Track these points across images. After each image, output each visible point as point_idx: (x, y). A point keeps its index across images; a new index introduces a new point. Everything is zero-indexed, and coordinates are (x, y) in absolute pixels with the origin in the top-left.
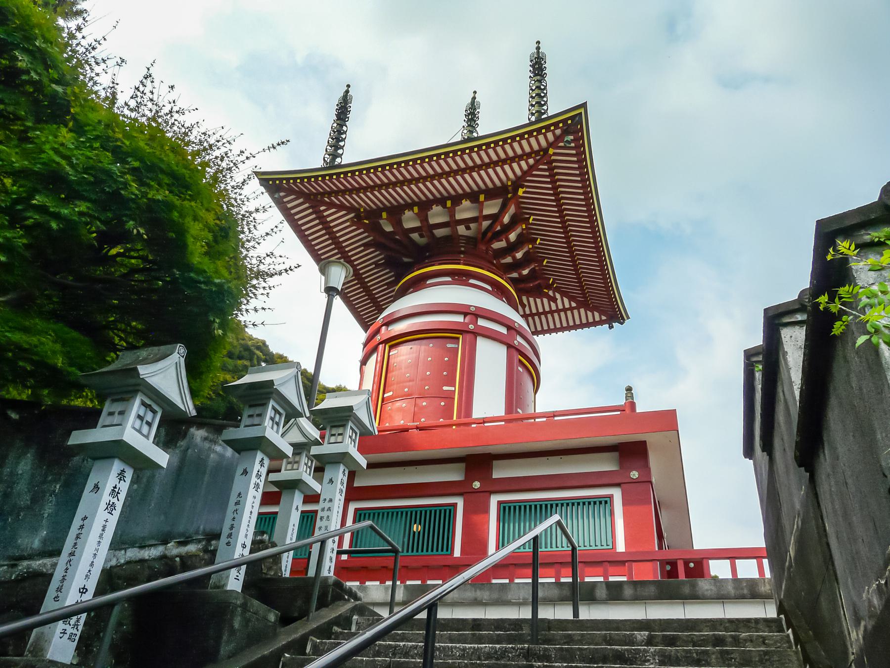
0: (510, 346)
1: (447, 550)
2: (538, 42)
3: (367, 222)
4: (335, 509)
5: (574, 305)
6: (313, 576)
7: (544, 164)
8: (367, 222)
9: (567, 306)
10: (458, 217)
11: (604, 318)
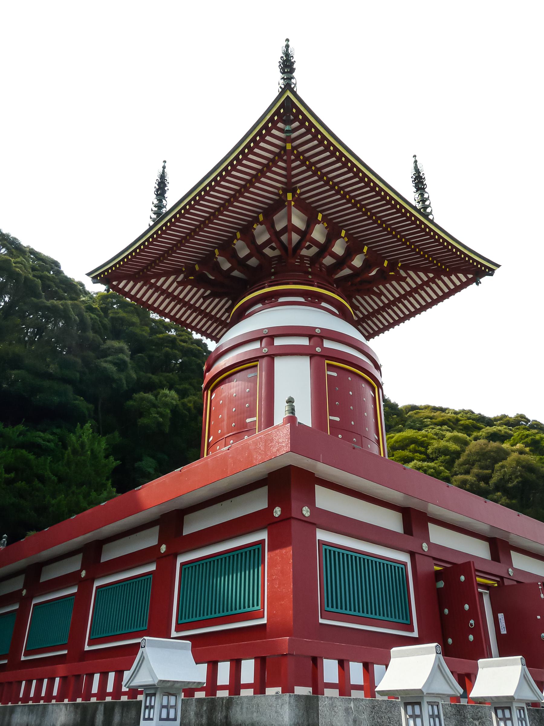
0: (312, 356)
1: (258, 605)
2: (287, 40)
3: (192, 278)
4: (124, 584)
5: (431, 275)
6: (146, 710)
7: (294, 161)
8: (192, 278)
9: (425, 279)
11: (470, 276)
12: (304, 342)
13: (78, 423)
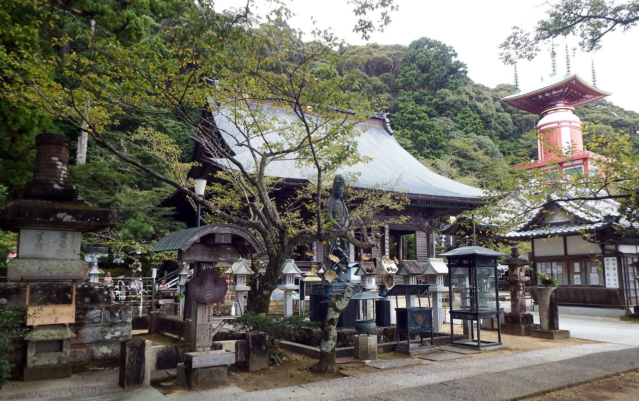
12: (568, 124)
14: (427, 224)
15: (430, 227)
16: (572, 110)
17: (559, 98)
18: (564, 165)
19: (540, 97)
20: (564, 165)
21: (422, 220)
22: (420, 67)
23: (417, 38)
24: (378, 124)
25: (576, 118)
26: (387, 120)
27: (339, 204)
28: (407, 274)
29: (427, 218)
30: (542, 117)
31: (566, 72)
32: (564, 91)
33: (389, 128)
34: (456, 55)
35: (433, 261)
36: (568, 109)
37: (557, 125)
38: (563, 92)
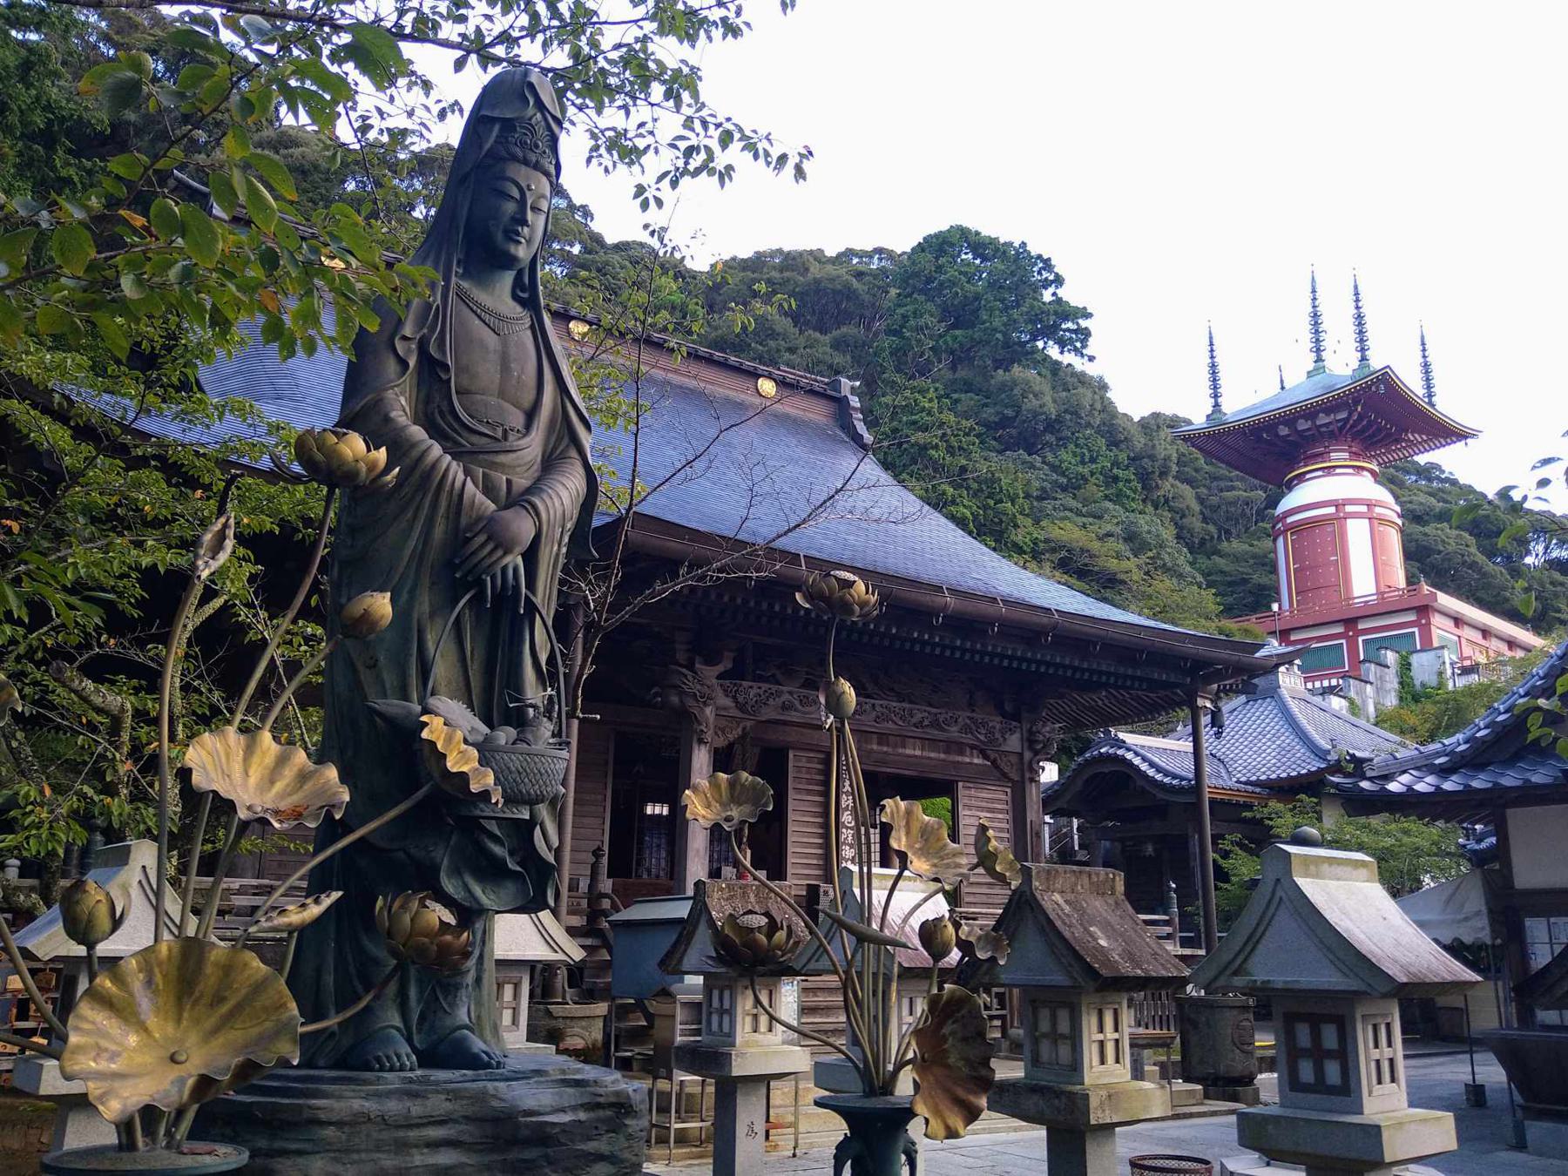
10: (1318, 423)
12: (1364, 509)
13: (1529, 560)
14: (1014, 742)
15: (1028, 755)
16: (1372, 472)
17: (1335, 435)
18: (1360, 627)
19: (1284, 431)
20: (1360, 627)
21: (996, 722)
22: (945, 312)
23: (939, 224)
24: (816, 412)
25: (1382, 494)
26: (855, 402)
27: (494, 323)
28: (1059, 978)
29: (1016, 717)
30: (1290, 486)
31: (1356, 364)
32: (1350, 415)
33: (861, 428)
34: (1059, 281)
35: (1312, 866)
36: (1363, 468)
37: (1332, 510)
38: (1346, 420)
